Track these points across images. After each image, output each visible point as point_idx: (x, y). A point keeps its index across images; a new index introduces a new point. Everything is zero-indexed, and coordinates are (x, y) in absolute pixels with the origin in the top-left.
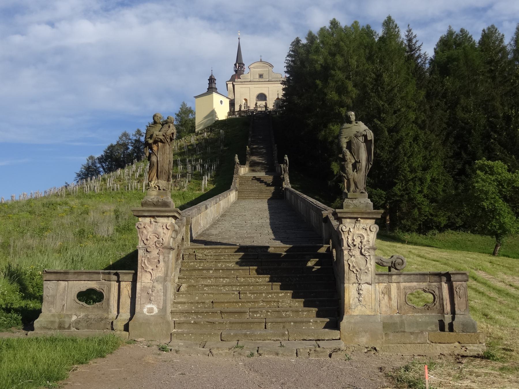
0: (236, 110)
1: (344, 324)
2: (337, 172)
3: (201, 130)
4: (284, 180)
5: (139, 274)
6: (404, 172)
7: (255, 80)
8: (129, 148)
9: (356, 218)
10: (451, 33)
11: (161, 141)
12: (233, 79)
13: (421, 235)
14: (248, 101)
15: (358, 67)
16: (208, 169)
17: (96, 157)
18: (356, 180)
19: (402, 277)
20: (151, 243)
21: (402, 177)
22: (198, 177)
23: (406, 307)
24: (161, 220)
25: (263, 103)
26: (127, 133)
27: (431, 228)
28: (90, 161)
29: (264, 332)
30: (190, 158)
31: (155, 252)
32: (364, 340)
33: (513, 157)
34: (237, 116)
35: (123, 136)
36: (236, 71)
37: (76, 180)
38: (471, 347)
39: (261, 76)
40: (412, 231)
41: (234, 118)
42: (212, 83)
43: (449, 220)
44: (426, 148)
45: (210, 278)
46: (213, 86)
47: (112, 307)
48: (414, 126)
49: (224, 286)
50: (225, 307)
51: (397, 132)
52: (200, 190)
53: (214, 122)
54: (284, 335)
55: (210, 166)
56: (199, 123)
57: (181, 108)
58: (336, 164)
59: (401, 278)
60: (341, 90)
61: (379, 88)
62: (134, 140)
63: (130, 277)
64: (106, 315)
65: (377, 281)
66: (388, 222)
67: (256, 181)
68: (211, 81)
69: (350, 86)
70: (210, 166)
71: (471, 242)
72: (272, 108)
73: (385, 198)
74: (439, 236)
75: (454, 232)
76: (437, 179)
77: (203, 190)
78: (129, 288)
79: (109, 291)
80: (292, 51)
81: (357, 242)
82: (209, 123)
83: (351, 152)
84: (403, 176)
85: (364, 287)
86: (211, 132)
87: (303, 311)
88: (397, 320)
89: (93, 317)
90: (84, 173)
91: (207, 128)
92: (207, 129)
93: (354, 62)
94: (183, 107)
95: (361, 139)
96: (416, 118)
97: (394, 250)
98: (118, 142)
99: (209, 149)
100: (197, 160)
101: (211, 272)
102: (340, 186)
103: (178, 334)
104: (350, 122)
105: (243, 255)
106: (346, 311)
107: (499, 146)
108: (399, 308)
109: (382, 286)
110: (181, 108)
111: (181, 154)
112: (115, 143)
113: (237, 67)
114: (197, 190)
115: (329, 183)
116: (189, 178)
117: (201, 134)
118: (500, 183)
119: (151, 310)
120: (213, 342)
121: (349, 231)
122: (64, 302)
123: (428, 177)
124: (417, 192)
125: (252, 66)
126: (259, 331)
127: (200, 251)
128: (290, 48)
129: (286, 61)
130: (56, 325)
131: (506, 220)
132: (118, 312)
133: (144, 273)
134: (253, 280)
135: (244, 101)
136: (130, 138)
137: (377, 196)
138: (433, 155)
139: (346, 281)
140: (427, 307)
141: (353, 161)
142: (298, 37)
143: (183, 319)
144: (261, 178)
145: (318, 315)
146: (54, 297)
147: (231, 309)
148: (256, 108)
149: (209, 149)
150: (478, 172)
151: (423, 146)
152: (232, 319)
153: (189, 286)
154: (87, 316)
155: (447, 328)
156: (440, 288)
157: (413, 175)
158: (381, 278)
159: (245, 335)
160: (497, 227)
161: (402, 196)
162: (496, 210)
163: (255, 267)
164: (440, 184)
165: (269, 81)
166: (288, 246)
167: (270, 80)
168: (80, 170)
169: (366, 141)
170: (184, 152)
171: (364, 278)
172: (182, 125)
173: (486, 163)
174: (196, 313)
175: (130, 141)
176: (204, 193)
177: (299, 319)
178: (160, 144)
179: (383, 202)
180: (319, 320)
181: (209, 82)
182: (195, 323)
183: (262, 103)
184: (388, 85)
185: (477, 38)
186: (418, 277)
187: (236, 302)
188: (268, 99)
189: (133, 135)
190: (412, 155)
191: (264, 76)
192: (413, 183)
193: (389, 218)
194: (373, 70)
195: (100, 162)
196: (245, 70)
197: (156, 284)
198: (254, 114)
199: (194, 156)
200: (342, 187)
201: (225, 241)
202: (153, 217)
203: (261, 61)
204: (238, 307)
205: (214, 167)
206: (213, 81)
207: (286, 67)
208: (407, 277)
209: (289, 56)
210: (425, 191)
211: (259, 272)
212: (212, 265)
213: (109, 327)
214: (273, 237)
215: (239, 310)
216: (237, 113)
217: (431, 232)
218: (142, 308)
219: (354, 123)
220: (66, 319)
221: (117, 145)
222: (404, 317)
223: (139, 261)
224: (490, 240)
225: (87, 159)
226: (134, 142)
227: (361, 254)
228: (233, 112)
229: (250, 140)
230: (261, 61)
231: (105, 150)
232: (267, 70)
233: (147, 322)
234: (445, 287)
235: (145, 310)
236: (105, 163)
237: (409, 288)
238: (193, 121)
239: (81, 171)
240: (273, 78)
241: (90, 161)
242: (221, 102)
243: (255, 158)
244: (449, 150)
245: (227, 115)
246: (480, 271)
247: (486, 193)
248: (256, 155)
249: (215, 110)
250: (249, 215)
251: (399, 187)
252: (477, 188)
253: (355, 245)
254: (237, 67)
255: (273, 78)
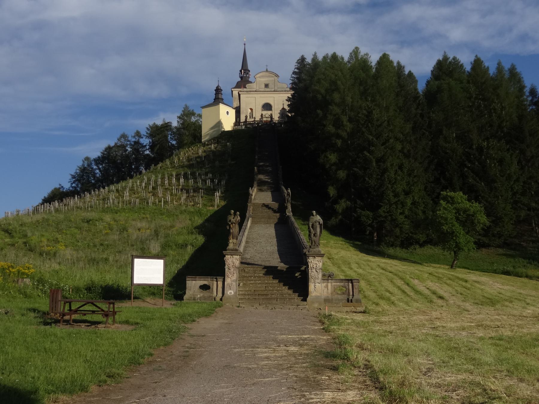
0: (241, 121)
1: (308, 299)
2: (333, 195)
3: (208, 141)
4: (287, 209)
5: (226, 278)
6: (388, 197)
7: (260, 90)
8: (127, 150)
9: (315, 257)
10: (445, 58)
11: (234, 223)
12: (238, 86)
13: (404, 250)
14: (254, 111)
15: (352, 102)
16: (218, 183)
17: (92, 159)
18: (315, 241)
19: (333, 281)
20: (231, 266)
21: (386, 201)
22: (210, 192)
23: (335, 293)
24: (235, 256)
25: (269, 113)
26: (126, 134)
27: (411, 244)
28: (85, 162)
29: (276, 302)
30: (200, 172)
31: (232, 270)
32: (316, 305)
33: (483, 184)
34: (243, 127)
35: (121, 137)
36: (241, 78)
37: (71, 181)
38: (358, 308)
39: (267, 86)
40: (396, 246)
41: (240, 130)
42: (219, 93)
43: (427, 237)
44: (409, 175)
45: (252, 281)
46: (220, 97)
47: (214, 292)
48: (401, 155)
49: (259, 284)
50: (260, 292)
51: (384, 162)
52: (213, 206)
53: (220, 133)
54: (284, 303)
55: (220, 181)
56: (206, 133)
57: (183, 111)
58: (332, 188)
59: (333, 281)
60: (338, 124)
61: (369, 124)
62: (133, 141)
63: (222, 280)
64: (212, 295)
65: (322, 282)
66: (376, 239)
67: (264, 208)
68: (218, 92)
69: (345, 119)
70: (220, 181)
71: (445, 256)
72: (278, 119)
73: (372, 218)
74: (419, 251)
75: (433, 247)
76: (418, 202)
77: (216, 206)
78: (221, 284)
79: (213, 285)
80: (297, 68)
81: (315, 266)
82: (216, 134)
83: (313, 229)
84: (387, 200)
85: (317, 284)
86: (218, 144)
87: (292, 294)
88: (330, 298)
89: (206, 296)
90: (79, 175)
91: (214, 139)
92: (214, 140)
93: (349, 99)
94: (185, 110)
95: (318, 223)
96: (403, 148)
97: (368, 264)
98: (116, 144)
99: (217, 163)
100: (206, 174)
101: (252, 278)
102: (334, 207)
103: (242, 302)
104: (313, 216)
105: (266, 271)
106: (309, 294)
107: (472, 174)
108: (332, 293)
109: (325, 284)
110: (183, 111)
111: (190, 166)
112: (112, 144)
113: (243, 74)
114: (210, 206)
115: (326, 204)
116: (201, 193)
117: (208, 145)
118: (458, 211)
119: (231, 293)
120: (257, 305)
121: (311, 262)
122: (195, 290)
123: (409, 202)
124: (398, 214)
125: (258, 76)
126: (274, 302)
127: (246, 268)
128: (295, 66)
129: (292, 78)
130: (193, 298)
131: (461, 240)
132: (217, 294)
133: (228, 278)
134: (271, 282)
135: (250, 111)
136: (129, 139)
137: (365, 217)
138: (416, 181)
139: (310, 282)
140: (343, 293)
141: (314, 233)
142: (303, 55)
143: (242, 297)
144: (268, 205)
145: (299, 296)
146: (191, 287)
147: (262, 293)
148: (262, 120)
149: (217, 163)
150: (442, 202)
151: (407, 173)
152: (263, 297)
153: (244, 284)
154: (204, 295)
155: (350, 301)
156: (348, 285)
157: (396, 200)
158: (324, 281)
159: (269, 303)
160: (454, 246)
161: (386, 217)
162: (453, 232)
163: (272, 276)
164: (420, 207)
165: (274, 91)
166: (287, 266)
167: (276, 90)
168: (75, 171)
169: (319, 224)
170: (193, 164)
171: (317, 281)
172: (184, 128)
173: (449, 194)
174: (248, 295)
175: (128, 143)
176: (217, 209)
177: (291, 297)
178: (234, 224)
179: (370, 222)
180: (299, 298)
181: (216, 92)
182: (248, 299)
183: (267, 113)
184: (378, 120)
185: (468, 68)
186: (340, 281)
187: (264, 291)
188: (273, 109)
189: (132, 137)
190: (395, 182)
191: (270, 86)
192: (396, 205)
193: (377, 235)
194: (365, 107)
195: (97, 164)
196: (250, 76)
197: (233, 282)
198: (260, 125)
199: (203, 169)
200: (336, 208)
201: (256, 263)
202: (232, 255)
203: (267, 71)
204: (265, 292)
205: (223, 182)
206: (220, 92)
207: (291, 84)
208: (335, 281)
209: (294, 73)
210: (407, 212)
211: (273, 278)
212: (253, 275)
213: (214, 300)
214: (279, 260)
215: (265, 294)
216: (243, 123)
217: (413, 247)
218: (227, 292)
219: (315, 216)
220: (196, 296)
221: (114, 146)
222: (333, 297)
223: (226, 272)
224: (449, 255)
225: (83, 160)
226: (133, 143)
227: (316, 271)
228: (239, 123)
229: (256, 157)
230: (267, 71)
231: (102, 151)
232: (272, 80)
233: (230, 297)
234: (350, 285)
235: (228, 293)
236: (102, 164)
237: (336, 285)
238: (199, 127)
239: (76, 173)
240: (279, 88)
241: (86, 162)
242: (228, 113)
243: (261, 177)
244: (430, 175)
245: (233, 125)
246: (416, 280)
247: (446, 219)
248: (263, 174)
249: (222, 121)
250: (264, 242)
251: (383, 209)
252: (439, 215)
253: (313, 268)
254: (243, 74)
255: (279, 88)
